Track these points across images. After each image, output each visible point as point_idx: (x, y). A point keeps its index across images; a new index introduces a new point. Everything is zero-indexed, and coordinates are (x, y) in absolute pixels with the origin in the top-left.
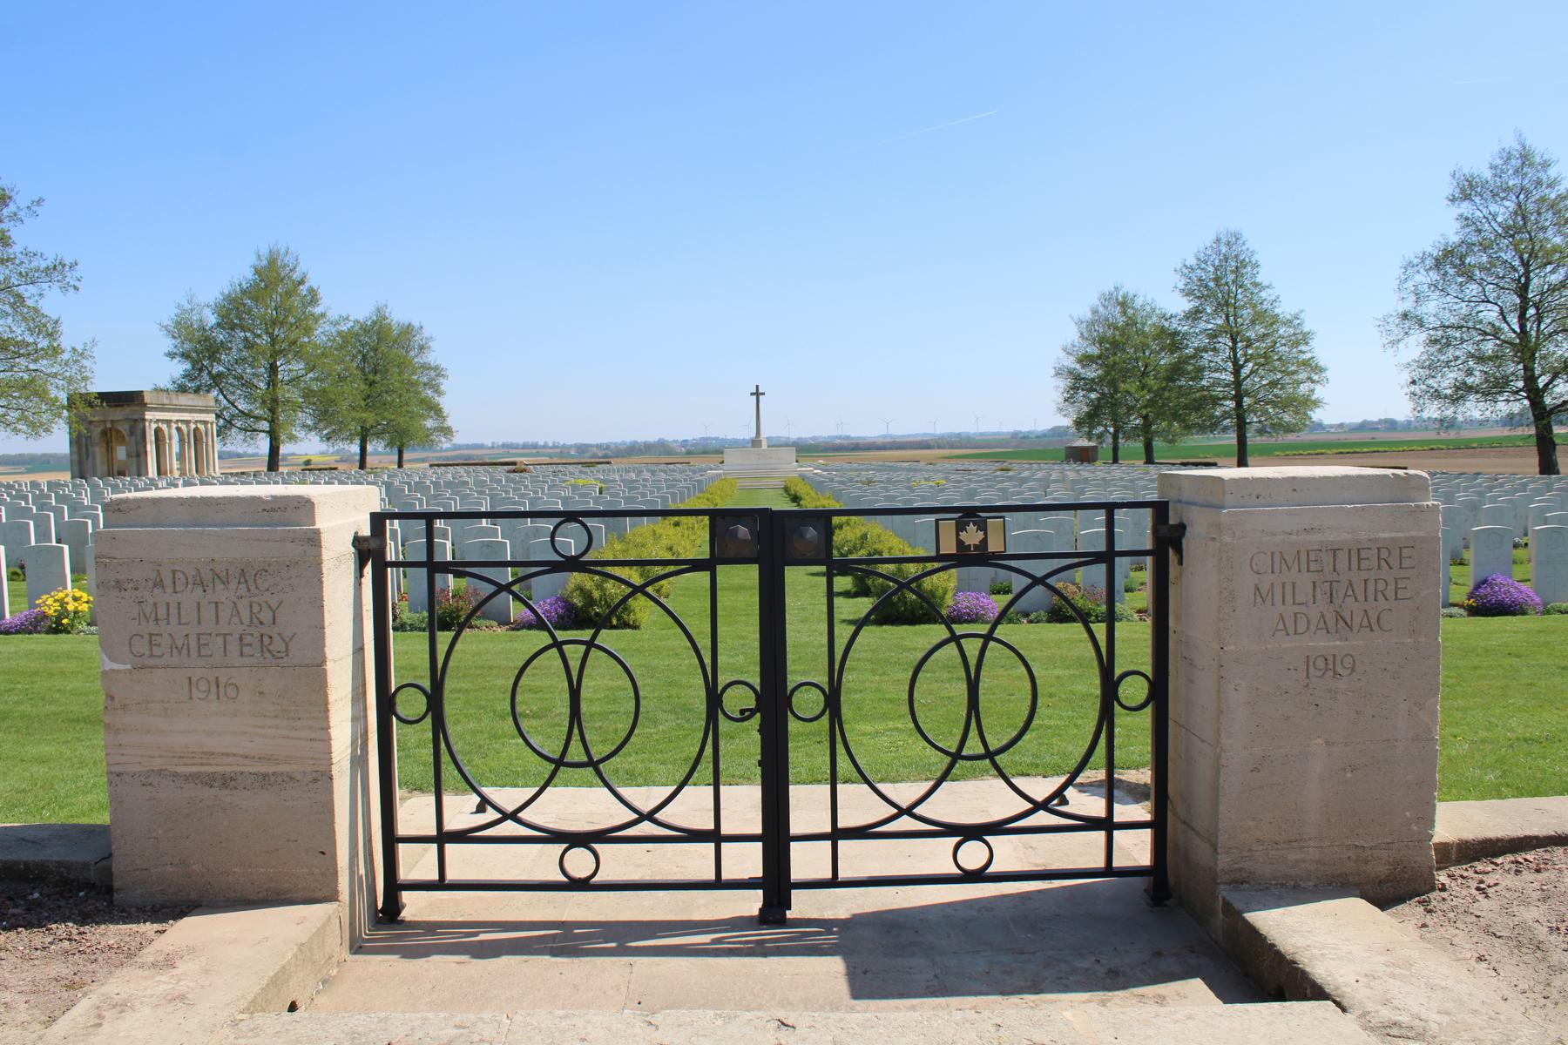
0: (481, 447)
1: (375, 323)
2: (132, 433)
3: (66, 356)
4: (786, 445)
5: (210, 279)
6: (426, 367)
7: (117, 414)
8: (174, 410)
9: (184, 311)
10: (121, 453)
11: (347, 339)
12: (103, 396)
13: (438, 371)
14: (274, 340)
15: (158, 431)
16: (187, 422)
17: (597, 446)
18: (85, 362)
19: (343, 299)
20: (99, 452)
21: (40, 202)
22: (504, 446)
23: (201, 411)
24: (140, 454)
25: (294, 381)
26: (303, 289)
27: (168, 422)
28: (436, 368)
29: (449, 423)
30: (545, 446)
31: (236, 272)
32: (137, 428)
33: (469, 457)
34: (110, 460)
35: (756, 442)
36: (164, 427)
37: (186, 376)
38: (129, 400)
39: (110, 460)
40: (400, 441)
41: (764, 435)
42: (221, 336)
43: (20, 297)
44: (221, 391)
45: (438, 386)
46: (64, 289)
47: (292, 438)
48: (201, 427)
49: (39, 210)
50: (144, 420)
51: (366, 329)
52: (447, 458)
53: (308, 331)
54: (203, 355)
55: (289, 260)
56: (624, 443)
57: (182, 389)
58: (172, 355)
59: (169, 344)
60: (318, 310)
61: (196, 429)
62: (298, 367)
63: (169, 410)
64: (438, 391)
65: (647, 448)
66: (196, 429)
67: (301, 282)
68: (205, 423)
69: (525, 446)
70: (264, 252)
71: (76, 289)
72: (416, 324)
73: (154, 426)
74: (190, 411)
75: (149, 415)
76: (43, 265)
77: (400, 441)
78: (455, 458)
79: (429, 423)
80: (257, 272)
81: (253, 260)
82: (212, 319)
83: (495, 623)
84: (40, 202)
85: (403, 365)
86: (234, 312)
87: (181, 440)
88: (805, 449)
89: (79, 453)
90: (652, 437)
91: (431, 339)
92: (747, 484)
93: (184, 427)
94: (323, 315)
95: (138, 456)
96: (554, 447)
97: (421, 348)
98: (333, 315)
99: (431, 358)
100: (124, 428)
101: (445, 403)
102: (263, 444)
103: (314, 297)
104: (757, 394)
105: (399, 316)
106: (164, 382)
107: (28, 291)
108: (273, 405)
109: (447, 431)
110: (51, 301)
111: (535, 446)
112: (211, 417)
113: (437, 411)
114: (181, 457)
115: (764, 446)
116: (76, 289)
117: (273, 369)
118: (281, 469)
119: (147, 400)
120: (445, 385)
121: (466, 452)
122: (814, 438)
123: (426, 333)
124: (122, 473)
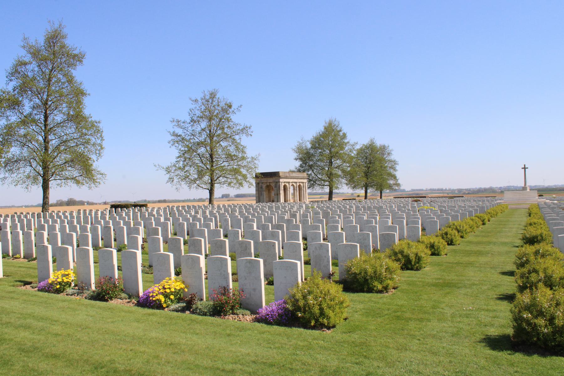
0: (422, 190)
1: (370, 145)
2: (276, 187)
3: (249, 160)
4: (535, 190)
5: (309, 132)
6: (390, 161)
7: (271, 180)
8: (291, 178)
9: (300, 144)
10: (273, 194)
11: (361, 151)
12: (262, 174)
13: (395, 162)
14: (331, 152)
15: (285, 186)
16: (296, 183)
17: (466, 189)
18: (255, 161)
19: (357, 138)
20: (265, 194)
21: (241, 106)
22: (430, 190)
23: (301, 179)
24: (278, 194)
25: (338, 167)
26: (341, 134)
27: (289, 183)
28: (394, 161)
29: (399, 182)
30: (446, 190)
31: (317, 128)
32: (277, 184)
33: (417, 194)
34: (269, 197)
35: (524, 188)
36: (287, 184)
37: (301, 166)
38: (275, 175)
39: (269, 197)
40: (380, 188)
41: (528, 184)
42: (312, 151)
43: (234, 139)
44: (313, 171)
45: (395, 168)
46: (247, 135)
47: (337, 188)
48: (302, 184)
49: (241, 109)
50: (279, 182)
51: (367, 147)
52: (410, 194)
53: (342, 148)
54: (306, 159)
55: (336, 123)
56: (476, 188)
57: (299, 171)
58: (296, 159)
59: (295, 155)
60: (346, 141)
61: (299, 186)
62: (339, 162)
63: (289, 178)
64: (395, 170)
65: (485, 190)
66: (299, 186)
67: (340, 131)
68: (303, 183)
69: (438, 190)
70: (328, 120)
71: (251, 135)
72: (387, 145)
73: (283, 184)
74: (297, 179)
75: (281, 180)
76: (241, 128)
77: (380, 188)
78: (412, 194)
79: (392, 182)
80: (325, 128)
81: (324, 124)
82: (309, 146)
83: (249, 312)
84: (241, 106)
85: (382, 160)
86: (317, 143)
87: (294, 189)
88: (542, 192)
89: (259, 194)
90: (487, 186)
91: (392, 150)
92: (514, 207)
93: (295, 184)
94: (348, 142)
95: (277, 195)
96: (449, 190)
97: (389, 154)
98: (352, 142)
99: (392, 157)
100: (273, 185)
101: (398, 174)
102: (327, 190)
103: (345, 136)
104: (525, 168)
105: (379, 143)
106: (293, 169)
107: (237, 137)
108: (330, 176)
109: (398, 185)
110: (244, 140)
111: (442, 190)
112: (305, 181)
113: (394, 177)
114: (294, 194)
115: (528, 190)
116: (251, 135)
117: (331, 163)
118: (334, 199)
119: (281, 175)
120: (398, 167)
121: (416, 192)
122: (555, 186)
123: (390, 148)
124: (273, 201)
